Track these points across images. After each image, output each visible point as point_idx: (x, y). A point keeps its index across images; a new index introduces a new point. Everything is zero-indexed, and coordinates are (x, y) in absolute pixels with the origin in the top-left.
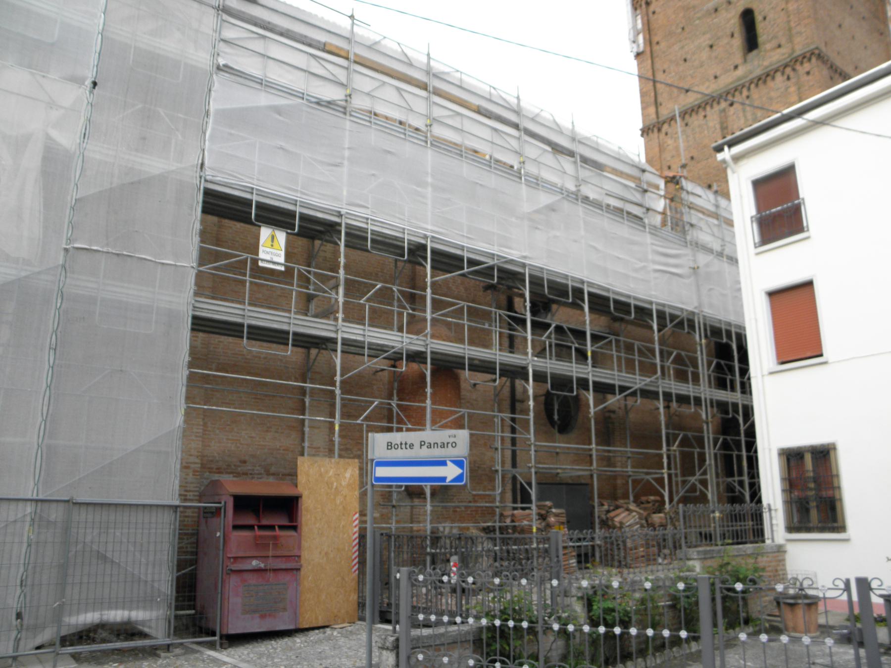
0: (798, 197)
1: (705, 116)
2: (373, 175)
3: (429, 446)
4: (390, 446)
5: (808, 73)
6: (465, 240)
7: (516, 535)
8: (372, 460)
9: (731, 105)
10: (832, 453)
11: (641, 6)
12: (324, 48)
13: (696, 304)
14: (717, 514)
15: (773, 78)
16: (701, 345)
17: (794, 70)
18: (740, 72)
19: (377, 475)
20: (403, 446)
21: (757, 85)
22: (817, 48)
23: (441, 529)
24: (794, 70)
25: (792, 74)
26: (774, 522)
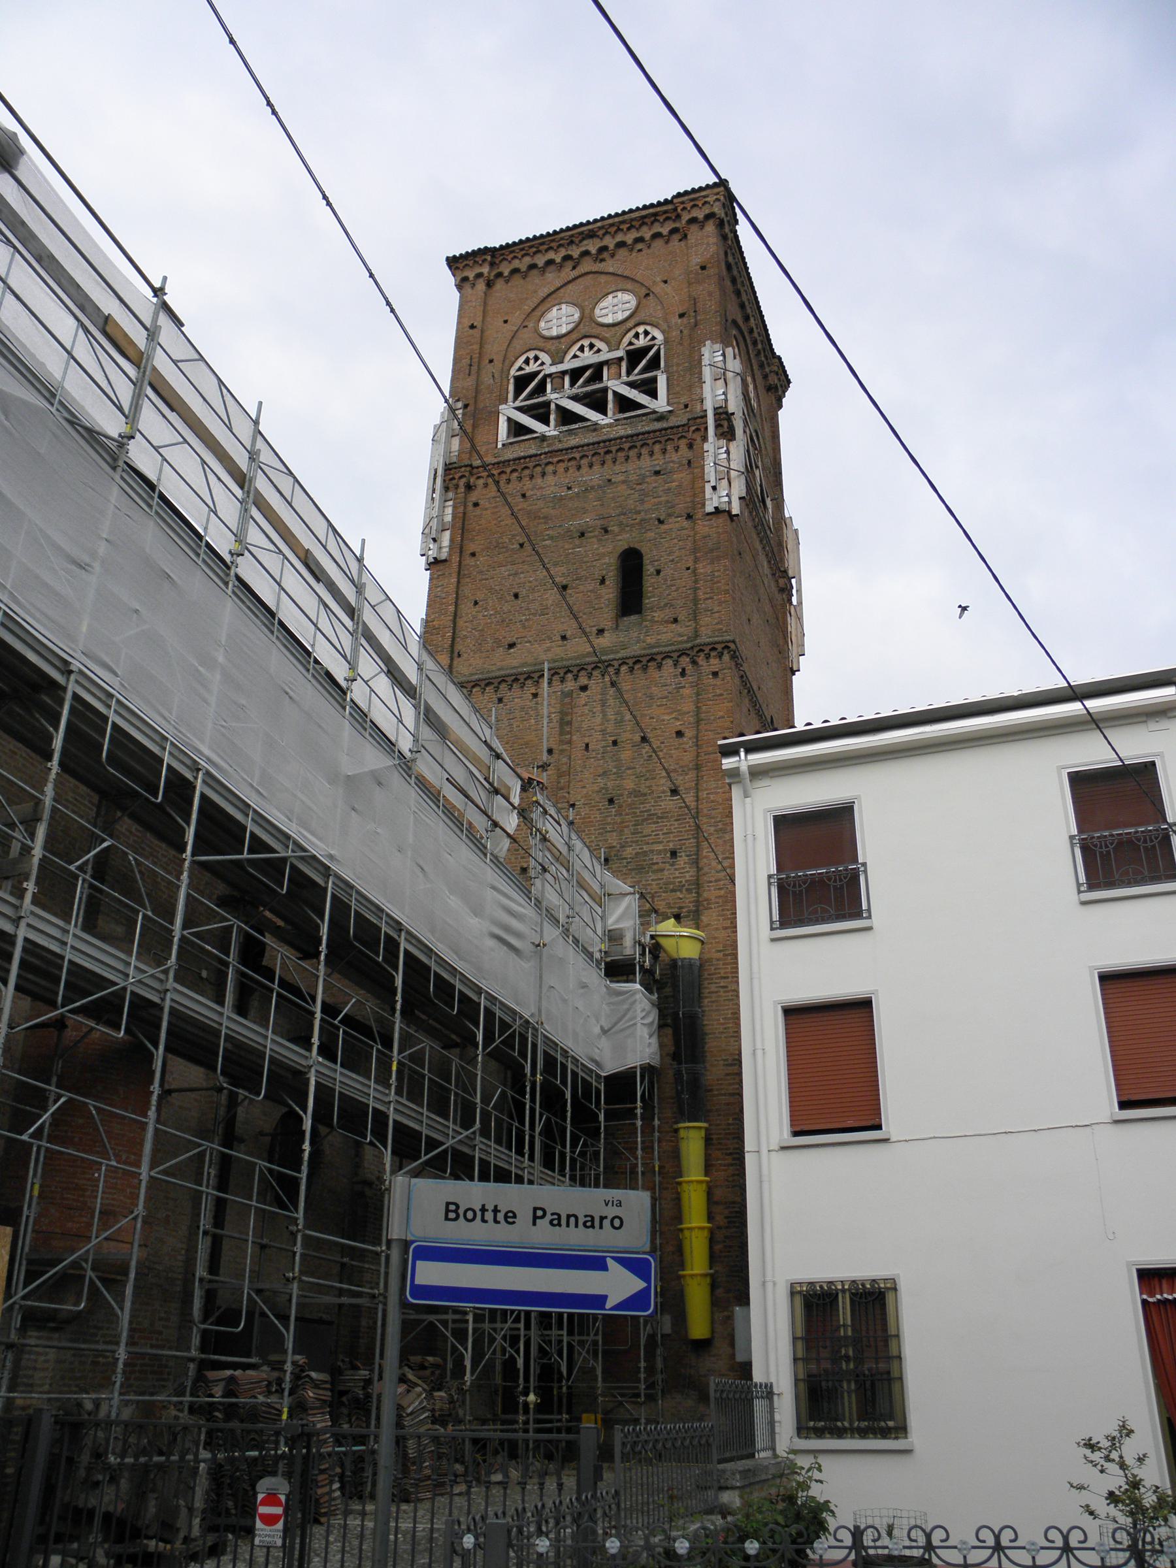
0: (855, 859)
1: (535, 695)
2: (137, 611)
3: (556, 1221)
4: (452, 1211)
5: (715, 674)
6: (254, 795)
7: (235, 1424)
8: (406, 1244)
9: (584, 688)
10: (890, 1297)
11: (457, 487)
12: (106, 325)
13: (533, 1010)
14: (532, 1398)
15: (659, 666)
16: (534, 1084)
17: (694, 662)
18: (604, 641)
19: (419, 1281)
20: (489, 1216)
21: (632, 670)
22: (734, 642)
23: (89, 1406)
24: (694, 662)
25: (689, 668)
26: (777, 1417)
